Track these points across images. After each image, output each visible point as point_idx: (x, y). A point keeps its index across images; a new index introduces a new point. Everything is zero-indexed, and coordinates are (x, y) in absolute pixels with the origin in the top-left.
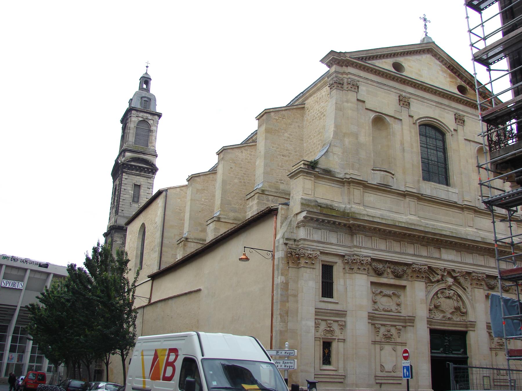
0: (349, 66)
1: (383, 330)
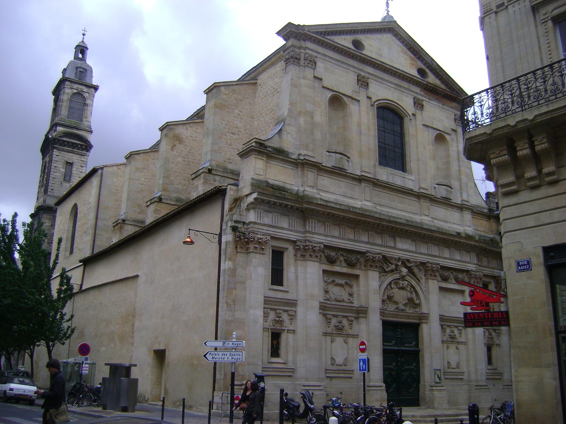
0: (307, 40)
1: (334, 321)
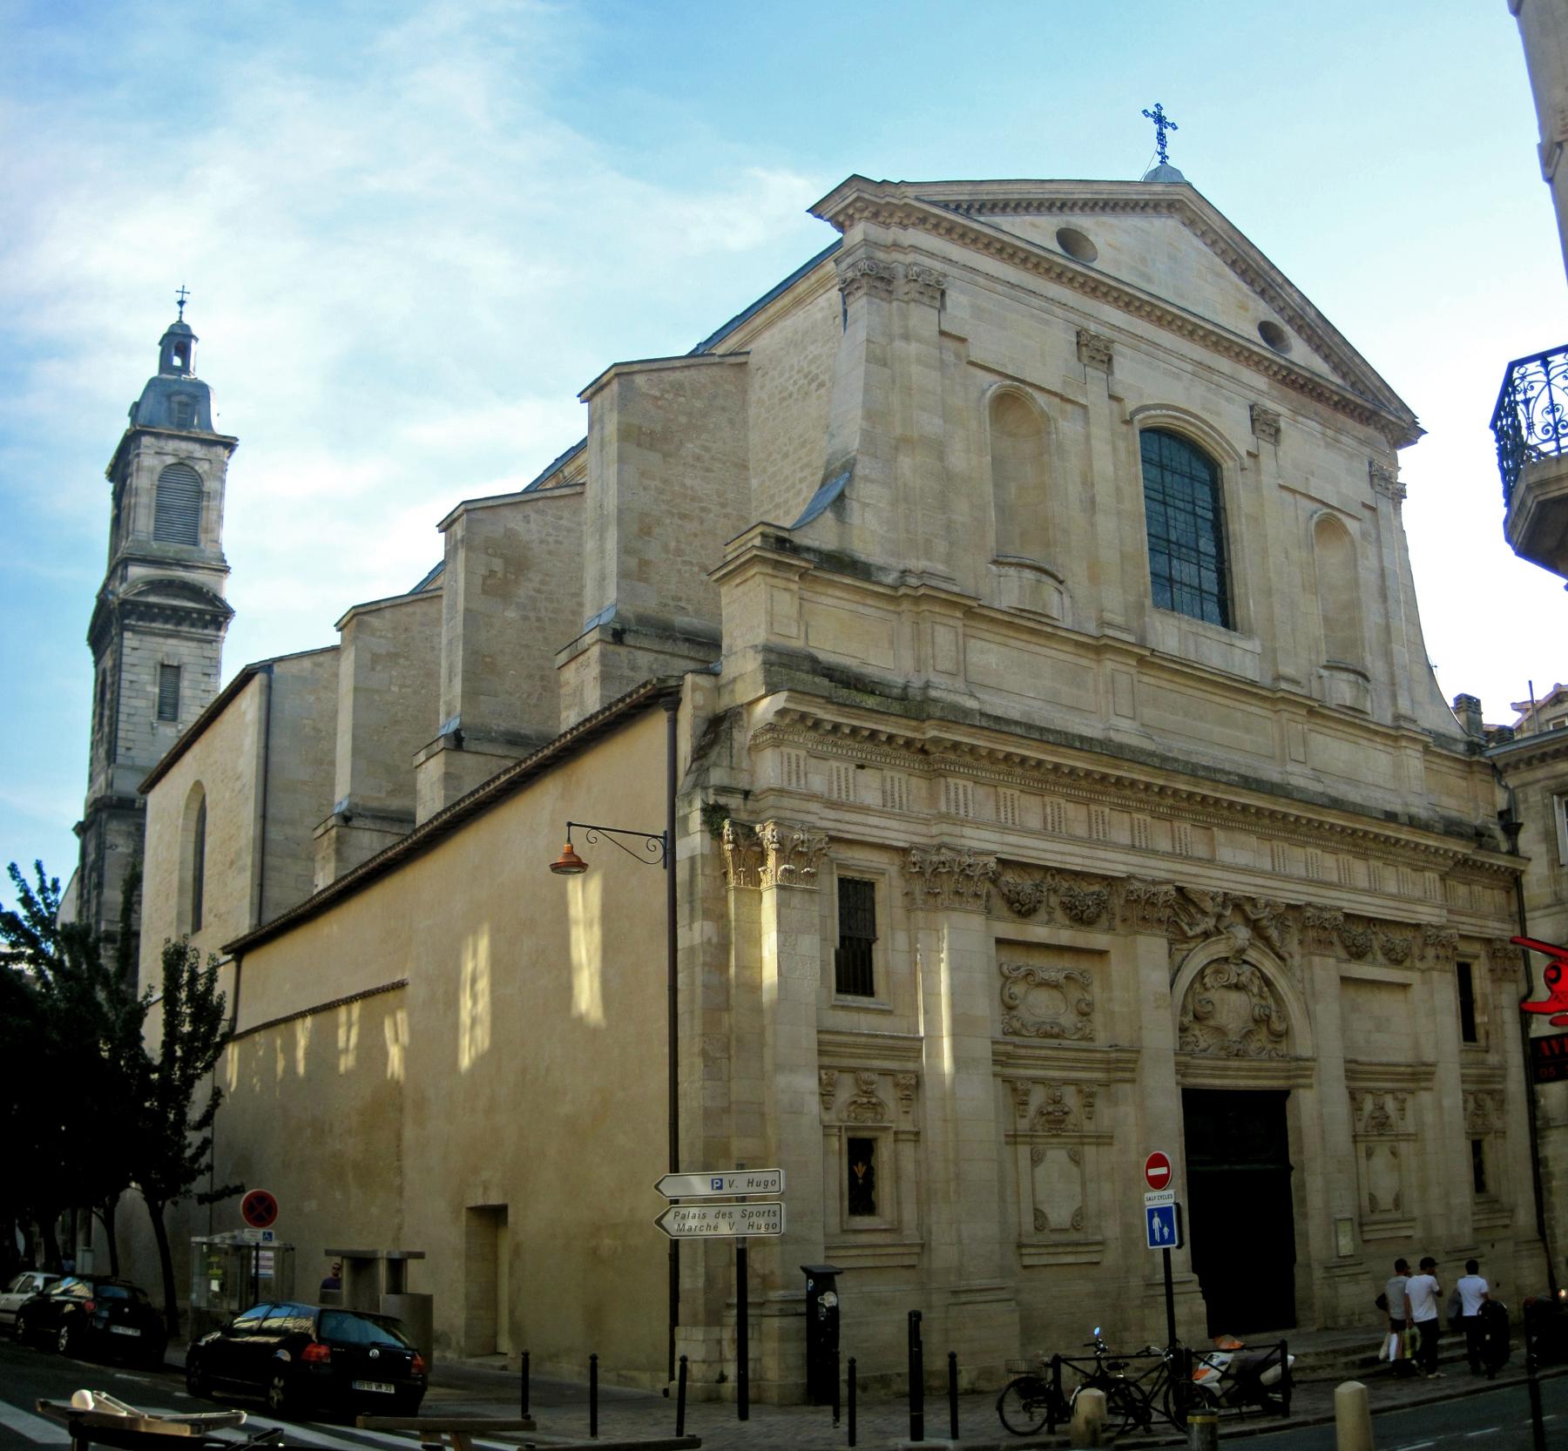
1: (1038, 1097)
